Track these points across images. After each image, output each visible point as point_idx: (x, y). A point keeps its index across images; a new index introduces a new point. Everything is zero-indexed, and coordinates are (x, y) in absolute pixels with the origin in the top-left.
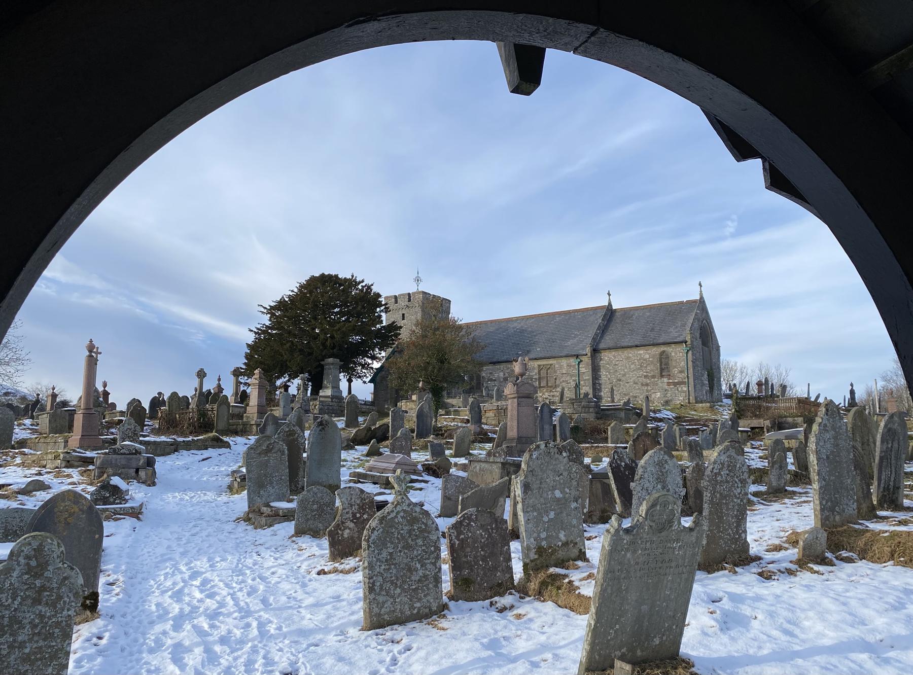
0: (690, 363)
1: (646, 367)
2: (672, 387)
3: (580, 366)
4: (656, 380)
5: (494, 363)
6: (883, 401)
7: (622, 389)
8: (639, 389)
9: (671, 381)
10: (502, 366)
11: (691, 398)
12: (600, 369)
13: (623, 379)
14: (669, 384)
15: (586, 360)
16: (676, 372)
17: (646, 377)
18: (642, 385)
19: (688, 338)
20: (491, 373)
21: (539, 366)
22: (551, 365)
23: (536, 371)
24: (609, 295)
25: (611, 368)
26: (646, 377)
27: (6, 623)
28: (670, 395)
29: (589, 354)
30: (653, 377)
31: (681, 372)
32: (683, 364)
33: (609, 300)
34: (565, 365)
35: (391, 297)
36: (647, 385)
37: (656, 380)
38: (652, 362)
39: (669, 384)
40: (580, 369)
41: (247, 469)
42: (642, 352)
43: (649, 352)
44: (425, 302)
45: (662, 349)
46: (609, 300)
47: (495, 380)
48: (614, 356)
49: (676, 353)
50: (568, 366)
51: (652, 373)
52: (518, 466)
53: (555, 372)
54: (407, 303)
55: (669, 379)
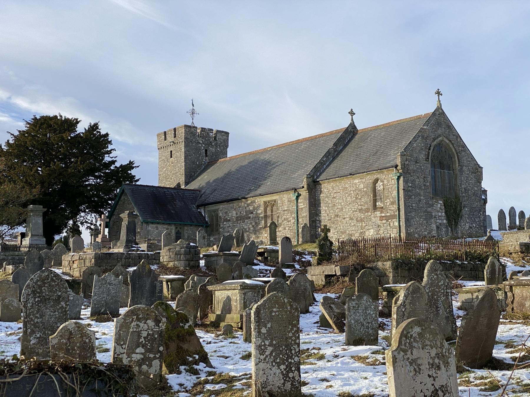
0: (401, 192)
1: (360, 199)
2: (384, 221)
3: (299, 201)
4: (370, 214)
5: (228, 201)
6: (392, 217)
7: (340, 226)
8: (354, 225)
9: (383, 215)
10: (235, 204)
11: (402, 234)
12: (320, 203)
13: (340, 214)
14: (381, 218)
15: (304, 193)
16: (388, 204)
17: (360, 210)
18: (357, 221)
19: (398, 161)
20: (226, 213)
21: (265, 203)
22: (275, 201)
23: (262, 208)
24: (438, 93)
25: (330, 202)
26: (360, 210)
27: (72, 135)
28: (382, 232)
29: (306, 187)
30: (367, 210)
31: (392, 203)
32: (395, 193)
33: (352, 120)
34: (286, 201)
35: (161, 133)
36: (362, 220)
37: (370, 214)
38: (366, 192)
39: (381, 218)
40: (299, 205)
41: (13, 277)
42: (356, 181)
43: (364, 180)
44: (189, 137)
45: (375, 177)
46: (352, 120)
47: (229, 220)
48: (333, 188)
49: (388, 181)
50: (289, 201)
51: (366, 206)
52: (125, 259)
53: (278, 209)
54: (173, 139)
55: (381, 213)
